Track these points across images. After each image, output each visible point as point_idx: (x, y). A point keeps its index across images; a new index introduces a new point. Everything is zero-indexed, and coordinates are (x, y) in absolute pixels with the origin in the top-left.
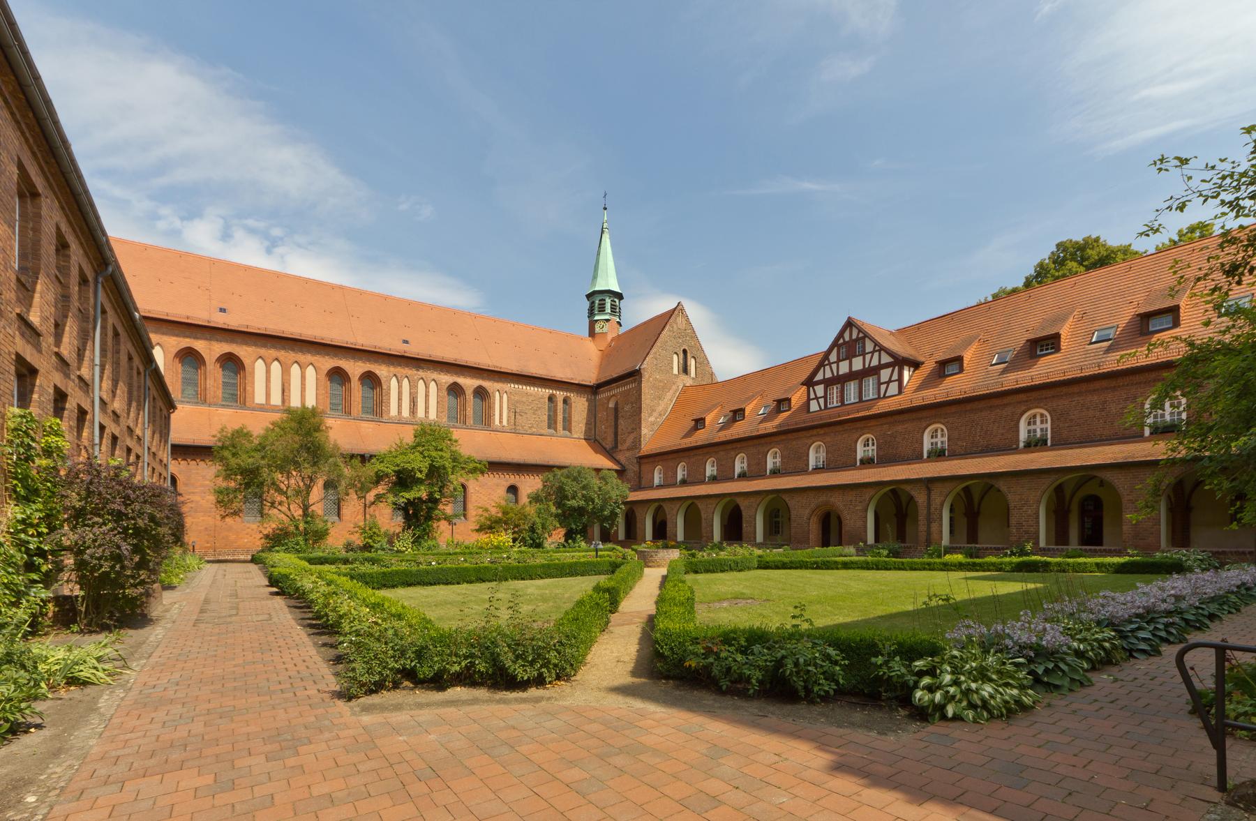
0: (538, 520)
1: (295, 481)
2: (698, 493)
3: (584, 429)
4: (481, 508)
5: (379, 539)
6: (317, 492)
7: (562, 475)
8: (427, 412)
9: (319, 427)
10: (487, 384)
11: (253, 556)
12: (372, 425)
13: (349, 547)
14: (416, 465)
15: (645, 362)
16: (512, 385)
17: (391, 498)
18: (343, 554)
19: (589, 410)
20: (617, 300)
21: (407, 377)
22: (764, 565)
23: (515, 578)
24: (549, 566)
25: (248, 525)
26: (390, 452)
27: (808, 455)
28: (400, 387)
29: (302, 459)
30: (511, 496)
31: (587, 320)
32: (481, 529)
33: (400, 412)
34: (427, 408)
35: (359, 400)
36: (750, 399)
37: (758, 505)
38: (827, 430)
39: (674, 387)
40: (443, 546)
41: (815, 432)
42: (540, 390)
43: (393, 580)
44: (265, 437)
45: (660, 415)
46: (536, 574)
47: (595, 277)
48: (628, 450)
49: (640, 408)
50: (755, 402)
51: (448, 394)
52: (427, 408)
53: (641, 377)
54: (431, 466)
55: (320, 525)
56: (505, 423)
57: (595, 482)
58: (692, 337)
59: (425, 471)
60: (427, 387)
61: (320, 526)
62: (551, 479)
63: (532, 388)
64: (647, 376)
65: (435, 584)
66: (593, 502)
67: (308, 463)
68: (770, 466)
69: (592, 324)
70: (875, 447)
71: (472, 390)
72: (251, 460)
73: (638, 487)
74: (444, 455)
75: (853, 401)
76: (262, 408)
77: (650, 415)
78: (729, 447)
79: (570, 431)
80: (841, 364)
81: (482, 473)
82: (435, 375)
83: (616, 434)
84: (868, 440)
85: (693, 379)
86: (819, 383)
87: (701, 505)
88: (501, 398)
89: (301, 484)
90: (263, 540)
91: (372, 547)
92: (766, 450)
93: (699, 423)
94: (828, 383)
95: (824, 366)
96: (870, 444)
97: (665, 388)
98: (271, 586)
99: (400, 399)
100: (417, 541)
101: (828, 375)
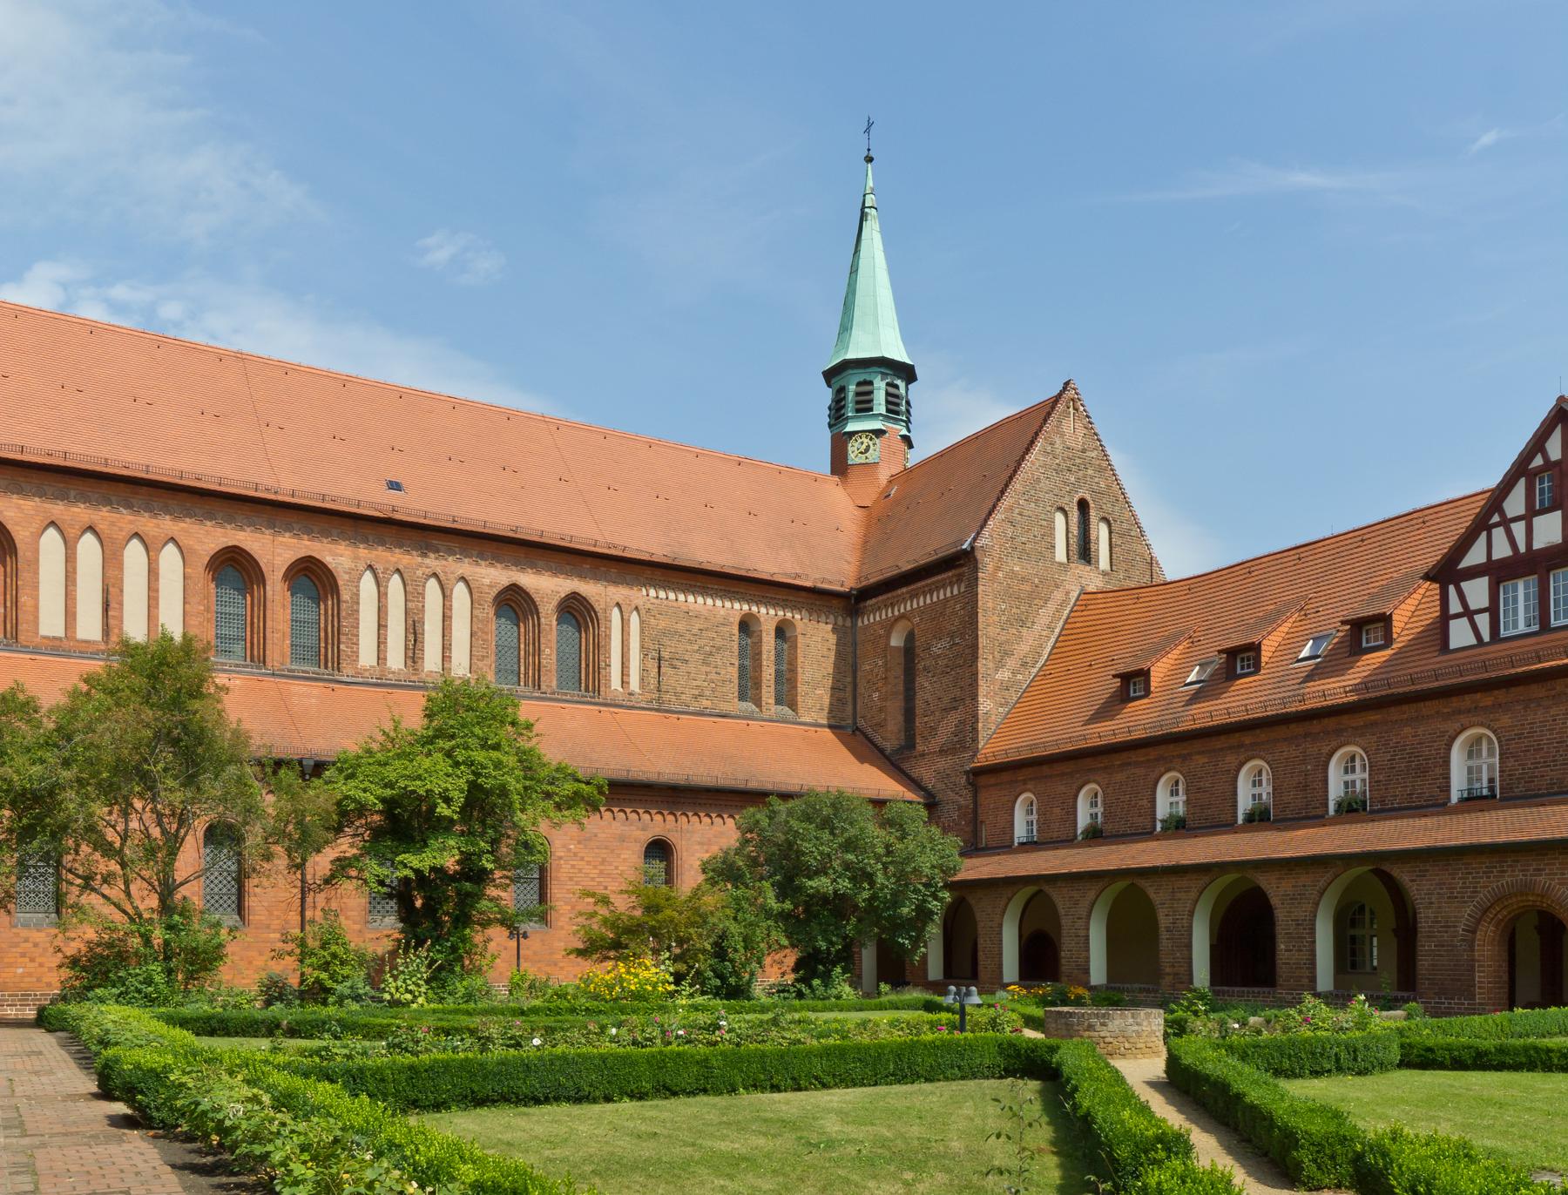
0: (734, 928)
1: (142, 820)
2: (1093, 866)
3: (826, 701)
4: (593, 895)
5: (346, 971)
6: (190, 856)
7: (790, 813)
8: (446, 657)
9: (200, 686)
10: (590, 589)
11: (41, 1011)
12: (316, 689)
13: (274, 992)
14: (436, 785)
15: (986, 532)
16: (652, 592)
17: (373, 868)
18: (256, 1010)
19: (839, 654)
20: (901, 384)
21: (398, 570)
22: (1420, 1059)
23: (756, 1086)
24: (841, 1053)
25: (24, 933)
26: (369, 752)
27: (1446, 763)
28: (382, 596)
29: (160, 766)
30: (658, 866)
31: (826, 436)
32: (592, 949)
33: (381, 658)
34: (446, 648)
35: (286, 627)
36: (1272, 619)
37: (1322, 894)
38: (1501, 695)
39: (1058, 595)
40: (501, 992)
41: (1467, 701)
42: (719, 603)
43: (436, 1088)
44: (73, 711)
45: (1024, 664)
46: (809, 1075)
47: (845, 327)
48: (943, 752)
49: (974, 647)
50: (1285, 628)
51: (498, 615)
52: (446, 648)
53: (976, 570)
54: (474, 787)
55: (200, 934)
56: (634, 684)
57: (877, 834)
58: (1101, 470)
59: (459, 798)
60: (446, 596)
61: (202, 937)
62: (765, 822)
63: (700, 600)
64: (990, 567)
65: (547, 1100)
66: (872, 883)
67: (176, 778)
68: (1335, 791)
69: (840, 443)
70: (1366, 775)
71: (555, 603)
72: (36, 769)
73: (973, 848)
74: (504, 759)
75: (1522, 628)
76: (57, 648)
77: (1000, 665)
78: (1219, 743)
79: (793, 705)
80: (1538, 521)
81: (594, 807)
82: (466, 567)
83: (909, 714)
84: (1353, 759)
85: (1104, 574)
86: (1474, 572)
87: (1157, 894)
88: (625, 623)
89: (156, 832)
90: (66, 973)
91: (328, 991)
92: (1326, 750)
93: (1133, 683)
94: (1499, 573)
95: (1489, 529)
96: (1485, 753)
97: (1036, 595)
98: (106, 1094)
99: (382, 626)
100: (438, 978)
101: (1502, 550)
